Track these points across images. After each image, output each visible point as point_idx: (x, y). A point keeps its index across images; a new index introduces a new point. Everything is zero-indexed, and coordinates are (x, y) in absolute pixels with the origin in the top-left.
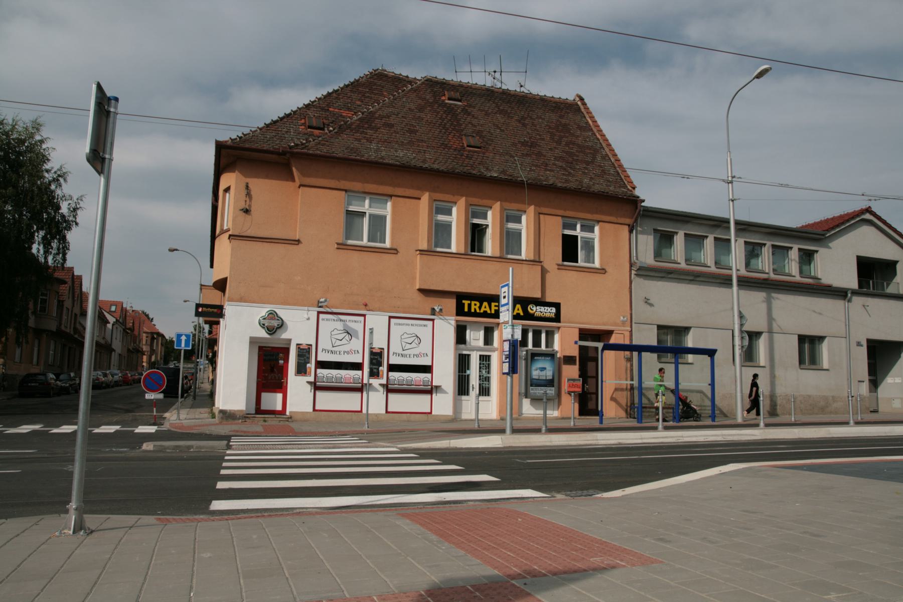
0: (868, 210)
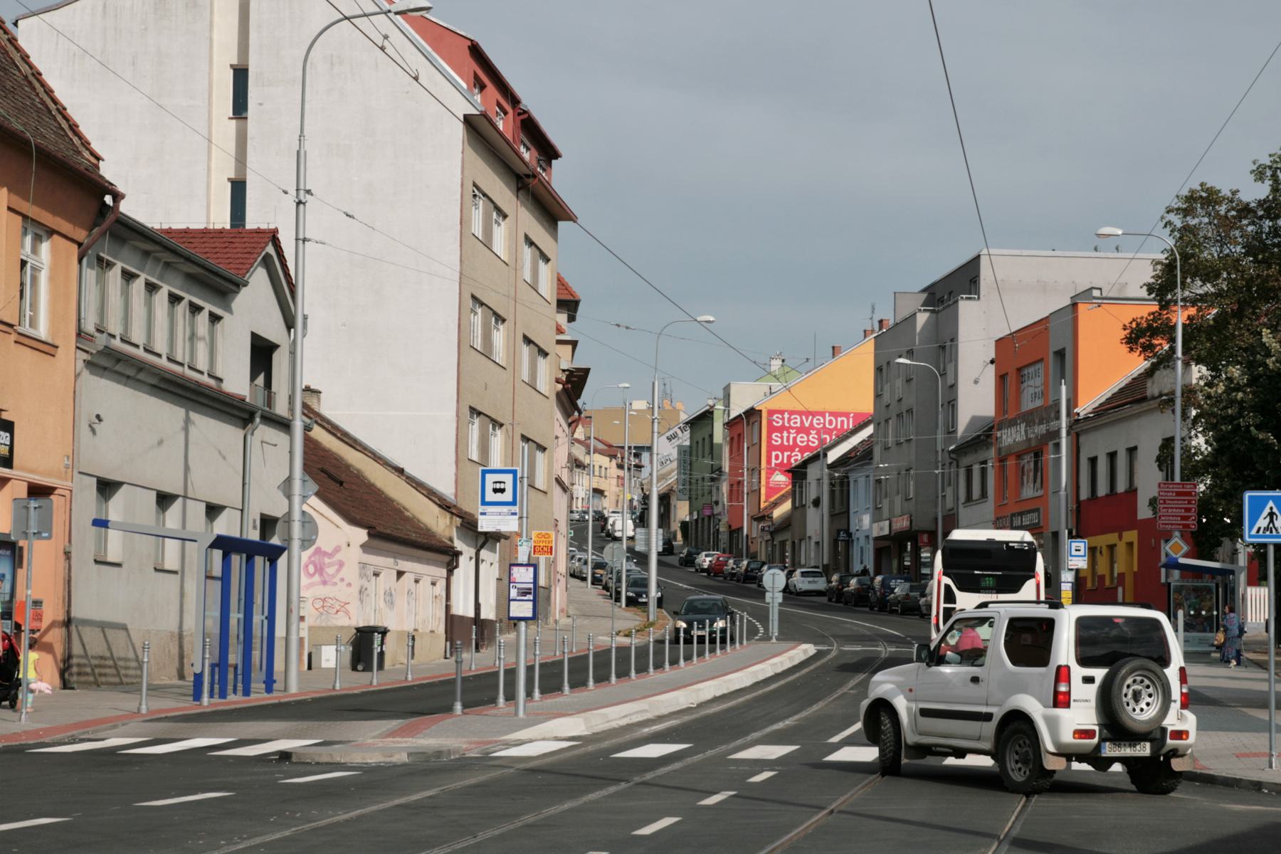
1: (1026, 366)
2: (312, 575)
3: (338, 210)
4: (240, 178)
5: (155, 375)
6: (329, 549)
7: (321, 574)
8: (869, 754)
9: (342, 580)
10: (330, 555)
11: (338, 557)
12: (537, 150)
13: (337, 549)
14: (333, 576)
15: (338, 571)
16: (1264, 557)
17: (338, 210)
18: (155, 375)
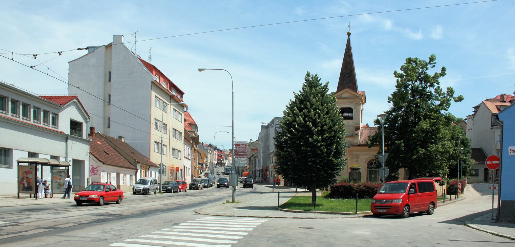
0: (76, 98)
1: (502, 132)
2: (92, 173)
3: (226, 132)
4: (20, 198)
5: (65, 135)
6: (95, 167)
7: (94, 173)
8: (181, 177)
9: (98, 174)
10: (95, 169)
11: (97, 169)
12: (163, 78)
13: (97, 167)
14: (96, 173)
15: (97, 172)
16: (459, 177)
17: (226, 132)
18: (65, 135)
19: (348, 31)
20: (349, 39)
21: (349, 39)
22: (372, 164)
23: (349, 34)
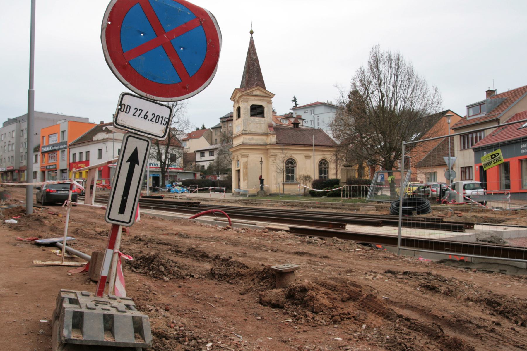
19: (251, 30)
20: (252, 37)
21: (252, 37)
22: (288, 162)
23: (252, 33)
